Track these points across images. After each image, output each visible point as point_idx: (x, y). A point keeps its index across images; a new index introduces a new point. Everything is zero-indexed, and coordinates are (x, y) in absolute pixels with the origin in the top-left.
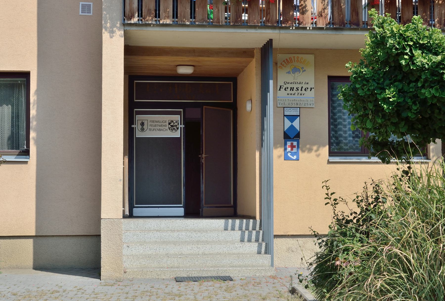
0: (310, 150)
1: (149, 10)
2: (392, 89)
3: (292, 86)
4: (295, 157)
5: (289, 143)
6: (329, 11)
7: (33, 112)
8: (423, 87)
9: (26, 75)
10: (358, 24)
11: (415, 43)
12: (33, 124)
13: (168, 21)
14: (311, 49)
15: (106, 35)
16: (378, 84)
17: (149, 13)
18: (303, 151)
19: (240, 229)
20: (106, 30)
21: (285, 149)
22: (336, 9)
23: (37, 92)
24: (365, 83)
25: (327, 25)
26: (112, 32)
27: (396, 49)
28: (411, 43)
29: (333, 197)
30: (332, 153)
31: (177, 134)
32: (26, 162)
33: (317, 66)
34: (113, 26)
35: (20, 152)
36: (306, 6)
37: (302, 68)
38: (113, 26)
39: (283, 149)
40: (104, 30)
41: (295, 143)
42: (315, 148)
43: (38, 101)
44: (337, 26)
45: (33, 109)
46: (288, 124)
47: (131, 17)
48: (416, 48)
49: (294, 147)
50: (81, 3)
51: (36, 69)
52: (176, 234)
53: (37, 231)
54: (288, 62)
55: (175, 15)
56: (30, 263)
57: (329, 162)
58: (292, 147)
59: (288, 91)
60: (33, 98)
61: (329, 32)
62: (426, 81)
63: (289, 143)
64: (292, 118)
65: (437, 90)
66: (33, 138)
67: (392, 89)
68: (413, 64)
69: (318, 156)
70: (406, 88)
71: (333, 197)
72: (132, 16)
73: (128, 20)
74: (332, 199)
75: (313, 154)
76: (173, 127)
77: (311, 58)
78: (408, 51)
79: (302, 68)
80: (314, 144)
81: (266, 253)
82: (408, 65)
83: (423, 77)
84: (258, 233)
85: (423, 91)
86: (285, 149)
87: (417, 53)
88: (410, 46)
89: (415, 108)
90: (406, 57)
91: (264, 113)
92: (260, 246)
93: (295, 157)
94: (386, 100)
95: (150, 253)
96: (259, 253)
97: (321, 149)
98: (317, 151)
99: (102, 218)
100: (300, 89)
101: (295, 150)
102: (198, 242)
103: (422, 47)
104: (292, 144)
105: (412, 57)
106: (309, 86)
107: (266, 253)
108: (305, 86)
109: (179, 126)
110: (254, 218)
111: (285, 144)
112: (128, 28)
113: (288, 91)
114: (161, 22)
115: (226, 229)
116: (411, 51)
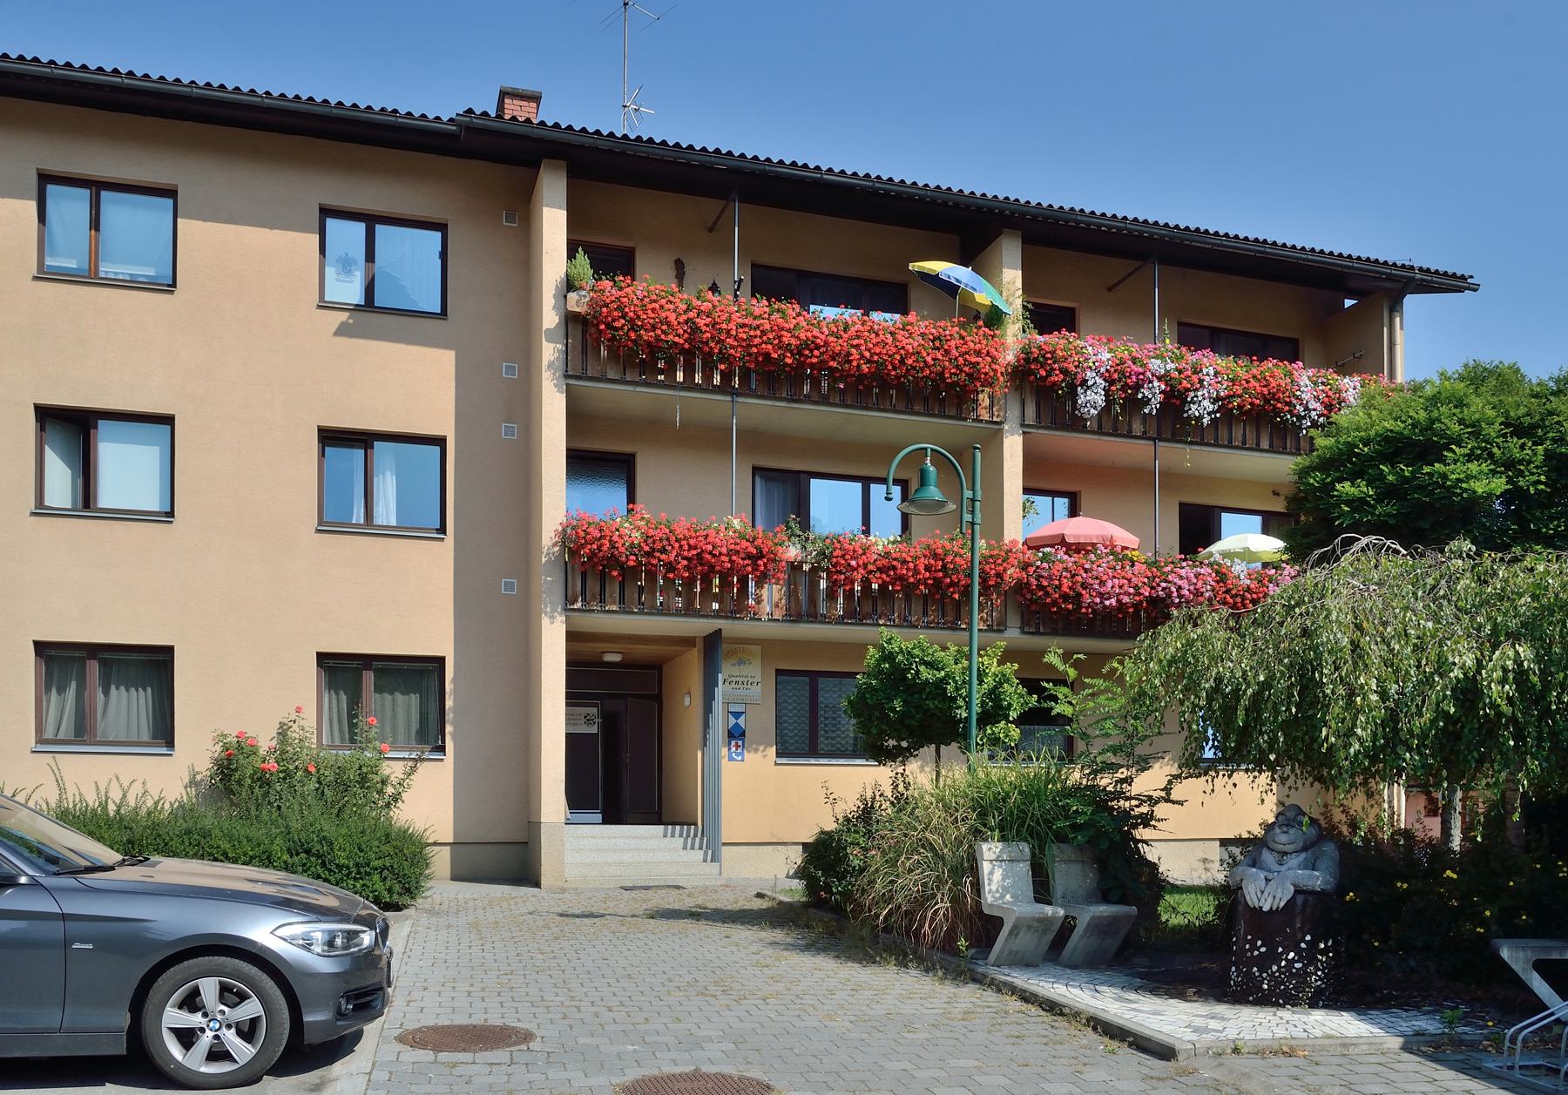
0: (756, 750)
1: (594, 595)
2: (899, 700)
3: (737, 679)
4: (740, 758)
5: (733, 743)
6: (783, 601)
7: (449, 703)
8: (927, 699)
9: (441, 661)
10: (816, 617)
11: (920, 660)
12: (449, 716)
13: (615, 608)
14: (757, 640)
15: (545, 621)
16: (885, 694)
17: (594, 599)
18: (749, 752)
19: (681, 836)
20: (546, 615)
21: (730, 749)
22: (792, 599)
23: (454, 680)
24: (874, 693)
25: (783, 616)
26: (552, 617)
27: (905, 664)
28: (917, 660)
29: (832, 797)
30: (779, 755)
31: (594, 730)
32: (171, 755)
33: (765, 657)
34: (553, 611)
35: (433, 748)
36: (762, 595)
37: (749, 660)
38: (553, 611)
39: (727, 749)
40: (543, 615)
41: (740, 743)
42: (761, 748)
43: (455, 690)
44: (794, 619)
45: (450, 699)
46: (732, 721)
47: (574, 601)
48: (921, 664)
49: (740, 746)
50: (503, 580)
51: (453, 653)
52: (613, 841)
53: (454, 838)
54: (733, 653)
55: (622, 601)
56: (448, 873)
57: (776, 764)
58: (737, 746)
59: (733, 685)
60: (449, 687)
61: (786, 624)
62: (930, 693)
63: (733, 743)
64: (737, 715)
65: (939, 702)
66: (450, 733)
67: (899, 700)
68: (919, 678)
69: (765, 756)
70: (909, 699)
71: (832, 797)
72: (575, 601)
73: (570, 605)
74: (831, 799)
75: (760, 754)
76: (589, 721)
77: (757, 649)
78: (914, 667)
79: (749, 660)
80: (760, 745)
81: (712, 861)
82: (914, 678)
83: (928, 690)
84: (702, 840)
85: (927, 702)
86: (730, 749)
87: (922, 668)
88: (916, 662)
89: (918, 716)
90: (912, 671)
91: (708, 709)
92: (706, 854)
93: (740, 758)
94: (893, 709)
95: (587, 861)
96: (705, 861)
97: (768, 749)
98: (763, 751)
99: (601, 815)
100: (745, 683)
101: (740, 750)
102: (637, 849)
103: (926, 663)
104: (737, 743)
105: (918, 672)
106: (756, 680)
107: (712, 861)
108: (751, 680)
109: (597, 720)
110: (696, 824)
111: (730, 744)
112: (570, 614)
113: (733, 685)
114: (607, 608)
115: (665, 836)
116: (917, 667)
